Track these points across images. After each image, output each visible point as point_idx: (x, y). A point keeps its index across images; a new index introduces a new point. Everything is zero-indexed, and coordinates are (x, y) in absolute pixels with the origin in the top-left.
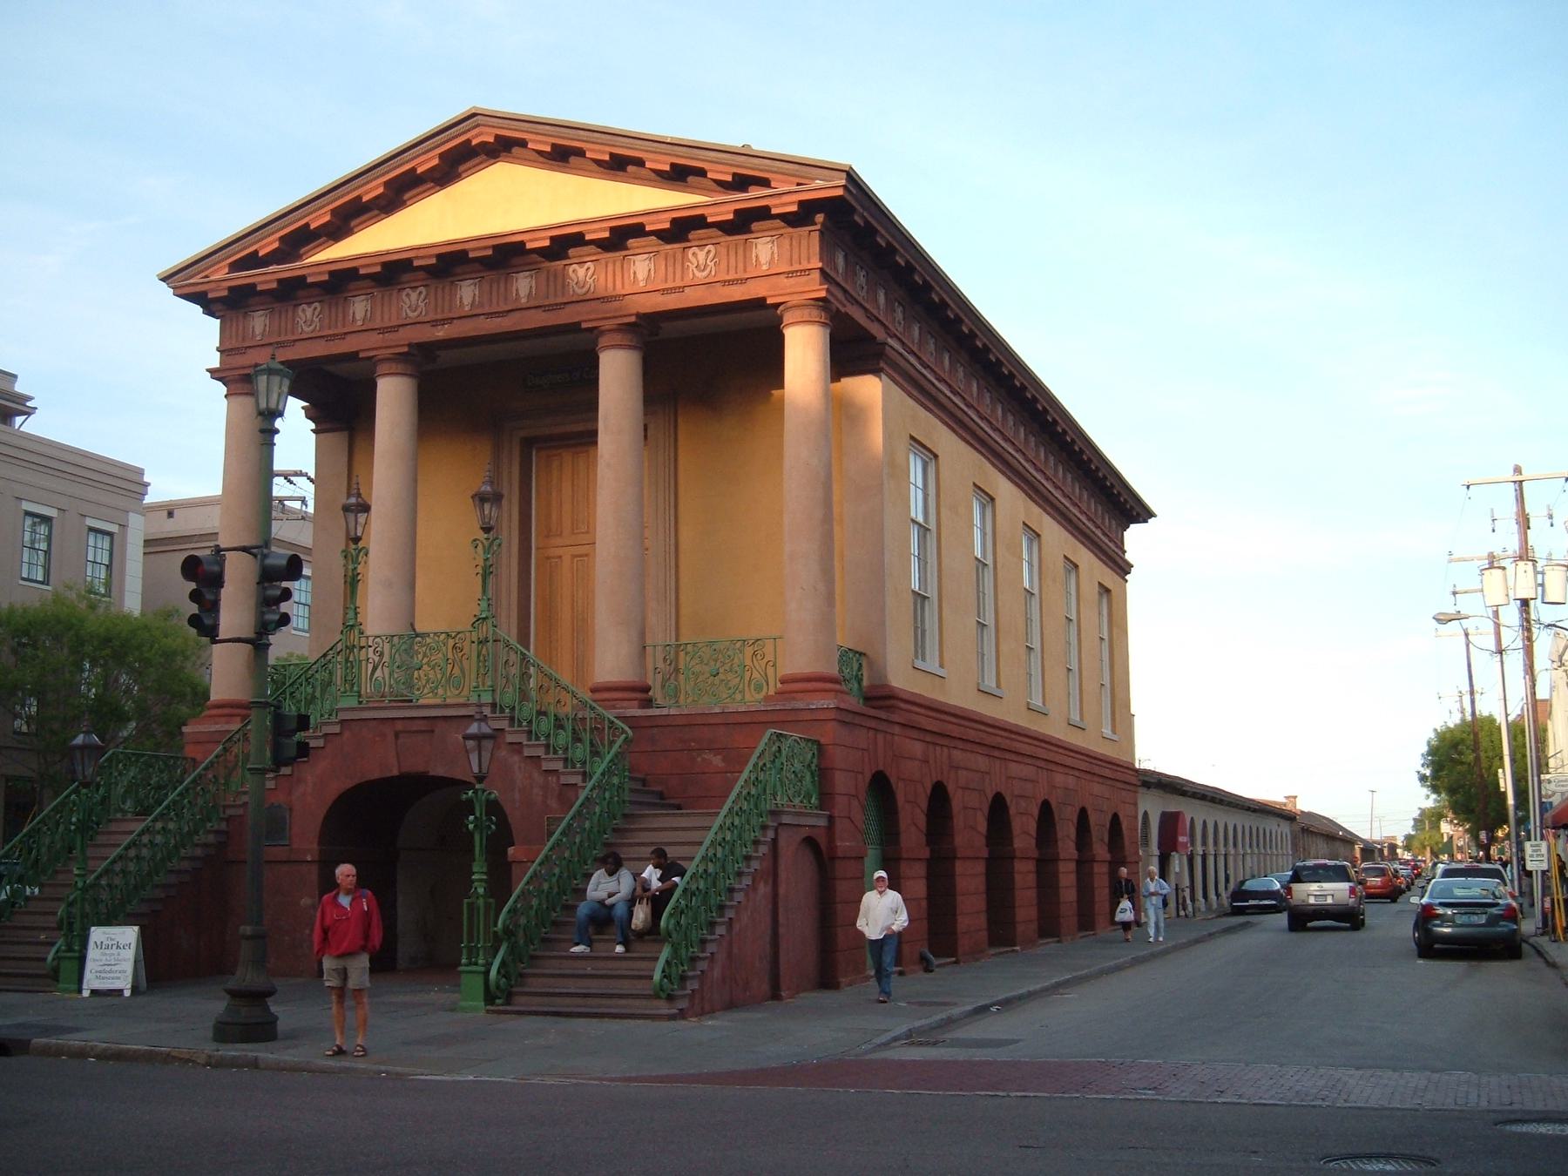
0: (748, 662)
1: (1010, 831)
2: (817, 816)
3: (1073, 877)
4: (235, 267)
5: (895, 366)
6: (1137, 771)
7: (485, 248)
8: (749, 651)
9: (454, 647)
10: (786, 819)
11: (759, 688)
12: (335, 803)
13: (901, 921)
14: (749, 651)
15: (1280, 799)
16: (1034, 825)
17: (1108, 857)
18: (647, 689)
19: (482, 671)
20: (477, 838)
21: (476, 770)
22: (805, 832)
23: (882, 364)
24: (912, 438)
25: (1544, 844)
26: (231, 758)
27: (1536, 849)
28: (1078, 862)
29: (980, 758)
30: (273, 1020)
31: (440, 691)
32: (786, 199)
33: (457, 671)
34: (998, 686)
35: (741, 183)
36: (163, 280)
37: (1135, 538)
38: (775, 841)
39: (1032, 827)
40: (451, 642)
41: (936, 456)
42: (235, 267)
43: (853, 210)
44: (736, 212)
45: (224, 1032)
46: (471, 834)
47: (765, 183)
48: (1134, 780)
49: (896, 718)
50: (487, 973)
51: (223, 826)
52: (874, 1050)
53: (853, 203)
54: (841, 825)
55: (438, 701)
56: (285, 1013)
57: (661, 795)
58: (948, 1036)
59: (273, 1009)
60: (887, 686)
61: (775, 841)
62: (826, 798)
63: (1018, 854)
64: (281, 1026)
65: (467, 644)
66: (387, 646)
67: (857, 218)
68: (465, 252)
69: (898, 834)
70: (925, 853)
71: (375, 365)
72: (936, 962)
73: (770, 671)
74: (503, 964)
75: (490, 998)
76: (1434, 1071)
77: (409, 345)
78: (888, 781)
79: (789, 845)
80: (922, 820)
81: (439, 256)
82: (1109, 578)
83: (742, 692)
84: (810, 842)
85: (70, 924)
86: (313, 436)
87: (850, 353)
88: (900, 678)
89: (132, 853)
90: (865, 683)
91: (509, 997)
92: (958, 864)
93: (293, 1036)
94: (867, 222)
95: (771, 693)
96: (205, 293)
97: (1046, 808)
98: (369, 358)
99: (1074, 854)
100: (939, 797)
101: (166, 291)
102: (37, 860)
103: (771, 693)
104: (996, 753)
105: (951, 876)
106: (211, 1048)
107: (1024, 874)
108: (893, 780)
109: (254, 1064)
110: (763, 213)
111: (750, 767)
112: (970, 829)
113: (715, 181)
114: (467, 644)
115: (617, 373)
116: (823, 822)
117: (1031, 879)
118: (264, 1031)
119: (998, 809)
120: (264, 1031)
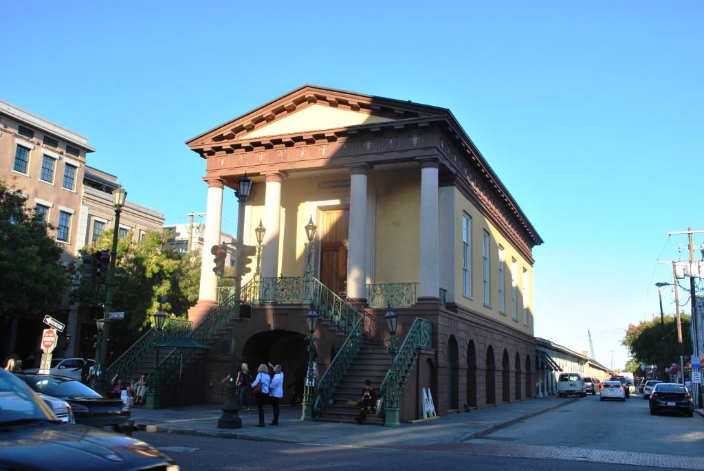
0: (405, 292)
3: (501, 378)
4: (216, 139)
5: (459, 184)
7: (426, 123)
8: (405, 288)
9: (297, 283)
10: (422, 351)
11: (409, 302)
13: (264, 391)
14: (405, 288)
15: (581, 353)
19: (307, 292)
20: (311, 354)
22: (428, 357)
23: (455, 183)
24: (464, 211)
25: (699, 373)
26: (209, 321)
27: (696, 375)
28: (516, 373)
31: (291, 299)
33: (297, 292)
34: (490, 304)
35: (407, 115)
36: (187, 144)
37: (536, 251)
39: (501, 358)
40: (295, 281)
41: (471, 218)
42: (216, 139)
43: (448, 125)
45: (221, 424)
47: (416, 115)
48: (533, 342)
49: (457, 315)
50: (313, 405)
52: (465, 439)
53: (448, 122)
54: (440, 355)
55: (290, 303)
58: (489, 436)
60: (454, 303)
62: (434, 343)
63: (440, 365)
65: (301, 283)
66: (271, 282)
67: (450, 128)
68: (369, 129)
72: (470, 408)
73: (414, 296)
74: (319, 402)
77: (366, 162)
78: (455, 338)
79: (423, 359)
80: (466, 354)
81: (358, 130)
82: (527, 265)
84: (429, 360)
85: (151, 383)
86: (238, 203)
87: (446, 179)
88: (460, 301)
89: (173, 357)
92: (460, 370)
94: (453, 130)
95: (414, 304)
96: (202, 149)
97: (490, 349)
98: (264, 175)
99: (525, 371)
100: (471, 345)
101: (188, 148)
103: (414, 304)
106: (218, 431)
108: (457, 338)
109: (235, 437)
110: (238, 146)
111: (410, 332)
113: (397, 113)
114: (301, 283)
115: (273, 189)
116: (433, 353)
118: (238, 424)
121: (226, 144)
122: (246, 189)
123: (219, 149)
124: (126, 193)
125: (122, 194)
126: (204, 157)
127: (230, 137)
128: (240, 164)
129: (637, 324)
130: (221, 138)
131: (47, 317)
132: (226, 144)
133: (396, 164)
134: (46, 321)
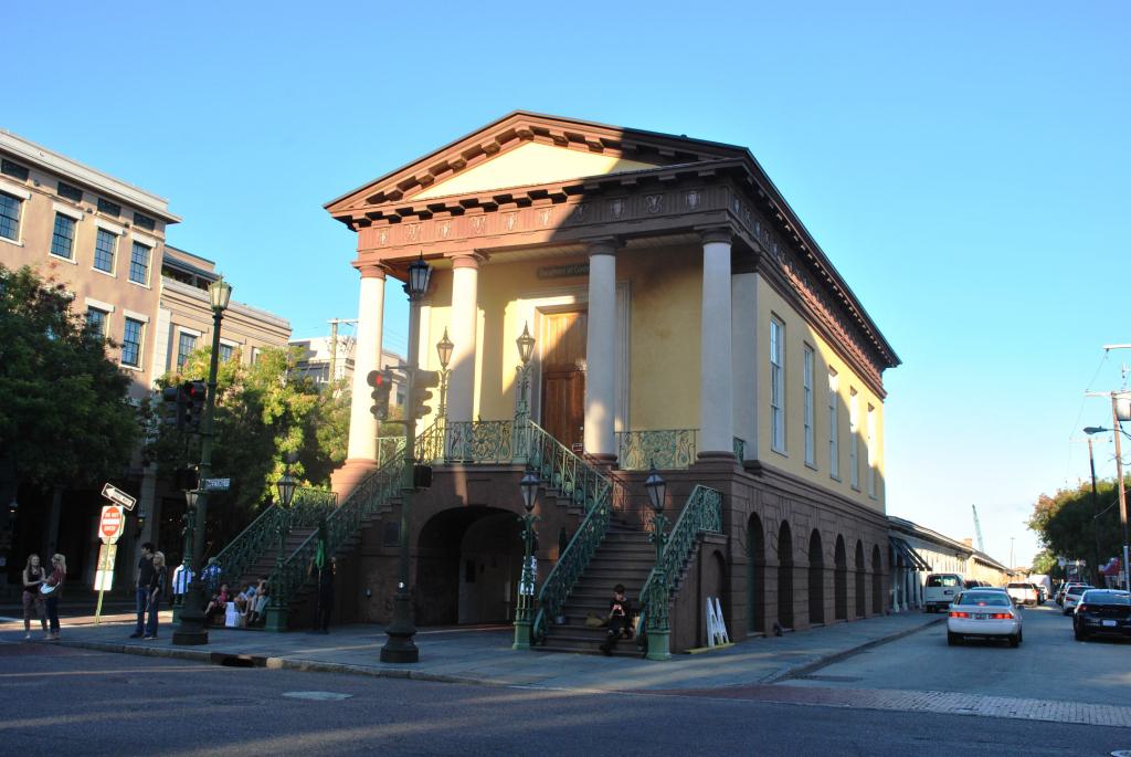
0: (678, 443)
1: (821, 552)
2: (722, 538)
4: (372, 200)
5: (765, 269)
6: (887, 518)
8: (678, 438)
9: (504, 430)
10: (706, 539)
11: (684, 460)
12: (430, 521)
14: (678, 438)
15: (962, 541)
16: (834, 550)
17: (872, 571)
18: (614, 458)
20: (527, 543)
21: (527, 504)
22: (715, 548)
24: (773, 312)
29: (806, 507)
30: (416, 651)
32: (670, 172)
34: (815, 462)
35: (679, 157)
37: (889, 377)
38: (700, 552)
40: (502, 427)
41: (784, 323)
42: (372, 200)
44: (677, 175)
45: (386, 656)
46: (524, 542)
47: (695, 158)
50: (532, 626)
51: (359, 534)
52: (778, 680)
54: (734, 545)
55: (494, 462)
56: (423, 647)
57: (624, 523)
59: (415, 643)
61: (700, 552)
62: (726, 527)
63: (767, 564)
64: (421, 652)
66: (463, 430)
69: (763, 551)
70: (778, 563)
71: (452, 261)
72: (783, 630)
73: (691, 449)
74: (542, 620)
75: (533, 640)
76: (848, 708)
78: (759, 519)
79: (708, 552)
82: (875, 401)
83: (674, 462)
84: (717, 553)
85: (274, 591)
88: (766, 459)
90: (745, 459)
91: (545, 641)
92: (766, 569)
93: (430, 658)
95: (692, 462)
96: (351, 217)
99: (833, 566)
101: (327, 215)
102: (248, 552)
103: (692, 462)
104: (815, 504)
105: (791, 578)
106: (381, 667)
107: (829, 580)
109: (408, 676)
110: (408, 212)
112: (828, 549)
113: (664, 156)
114: (511, 429)
115: (465, 280)
116: (724, 542)
117: (805, 583)
118: (411, 656)
119: (815, 538)
120: (411, 656)
121: (388, 209)
122: (422, 279)
123: (378, 216)
124: (230, 289)
125: (225, 291)
126: (354, 230)
127: (396, 196)
128: (411, 240)
129: (1052, 495)
130: (380, 198)
131: (109, 487)
132: (388, 209)
133: (516, 253)
134: (105, 493)
